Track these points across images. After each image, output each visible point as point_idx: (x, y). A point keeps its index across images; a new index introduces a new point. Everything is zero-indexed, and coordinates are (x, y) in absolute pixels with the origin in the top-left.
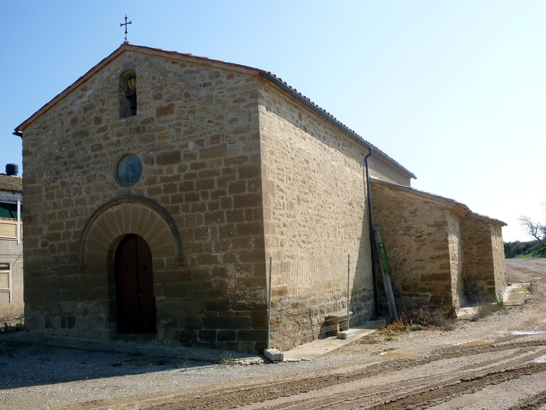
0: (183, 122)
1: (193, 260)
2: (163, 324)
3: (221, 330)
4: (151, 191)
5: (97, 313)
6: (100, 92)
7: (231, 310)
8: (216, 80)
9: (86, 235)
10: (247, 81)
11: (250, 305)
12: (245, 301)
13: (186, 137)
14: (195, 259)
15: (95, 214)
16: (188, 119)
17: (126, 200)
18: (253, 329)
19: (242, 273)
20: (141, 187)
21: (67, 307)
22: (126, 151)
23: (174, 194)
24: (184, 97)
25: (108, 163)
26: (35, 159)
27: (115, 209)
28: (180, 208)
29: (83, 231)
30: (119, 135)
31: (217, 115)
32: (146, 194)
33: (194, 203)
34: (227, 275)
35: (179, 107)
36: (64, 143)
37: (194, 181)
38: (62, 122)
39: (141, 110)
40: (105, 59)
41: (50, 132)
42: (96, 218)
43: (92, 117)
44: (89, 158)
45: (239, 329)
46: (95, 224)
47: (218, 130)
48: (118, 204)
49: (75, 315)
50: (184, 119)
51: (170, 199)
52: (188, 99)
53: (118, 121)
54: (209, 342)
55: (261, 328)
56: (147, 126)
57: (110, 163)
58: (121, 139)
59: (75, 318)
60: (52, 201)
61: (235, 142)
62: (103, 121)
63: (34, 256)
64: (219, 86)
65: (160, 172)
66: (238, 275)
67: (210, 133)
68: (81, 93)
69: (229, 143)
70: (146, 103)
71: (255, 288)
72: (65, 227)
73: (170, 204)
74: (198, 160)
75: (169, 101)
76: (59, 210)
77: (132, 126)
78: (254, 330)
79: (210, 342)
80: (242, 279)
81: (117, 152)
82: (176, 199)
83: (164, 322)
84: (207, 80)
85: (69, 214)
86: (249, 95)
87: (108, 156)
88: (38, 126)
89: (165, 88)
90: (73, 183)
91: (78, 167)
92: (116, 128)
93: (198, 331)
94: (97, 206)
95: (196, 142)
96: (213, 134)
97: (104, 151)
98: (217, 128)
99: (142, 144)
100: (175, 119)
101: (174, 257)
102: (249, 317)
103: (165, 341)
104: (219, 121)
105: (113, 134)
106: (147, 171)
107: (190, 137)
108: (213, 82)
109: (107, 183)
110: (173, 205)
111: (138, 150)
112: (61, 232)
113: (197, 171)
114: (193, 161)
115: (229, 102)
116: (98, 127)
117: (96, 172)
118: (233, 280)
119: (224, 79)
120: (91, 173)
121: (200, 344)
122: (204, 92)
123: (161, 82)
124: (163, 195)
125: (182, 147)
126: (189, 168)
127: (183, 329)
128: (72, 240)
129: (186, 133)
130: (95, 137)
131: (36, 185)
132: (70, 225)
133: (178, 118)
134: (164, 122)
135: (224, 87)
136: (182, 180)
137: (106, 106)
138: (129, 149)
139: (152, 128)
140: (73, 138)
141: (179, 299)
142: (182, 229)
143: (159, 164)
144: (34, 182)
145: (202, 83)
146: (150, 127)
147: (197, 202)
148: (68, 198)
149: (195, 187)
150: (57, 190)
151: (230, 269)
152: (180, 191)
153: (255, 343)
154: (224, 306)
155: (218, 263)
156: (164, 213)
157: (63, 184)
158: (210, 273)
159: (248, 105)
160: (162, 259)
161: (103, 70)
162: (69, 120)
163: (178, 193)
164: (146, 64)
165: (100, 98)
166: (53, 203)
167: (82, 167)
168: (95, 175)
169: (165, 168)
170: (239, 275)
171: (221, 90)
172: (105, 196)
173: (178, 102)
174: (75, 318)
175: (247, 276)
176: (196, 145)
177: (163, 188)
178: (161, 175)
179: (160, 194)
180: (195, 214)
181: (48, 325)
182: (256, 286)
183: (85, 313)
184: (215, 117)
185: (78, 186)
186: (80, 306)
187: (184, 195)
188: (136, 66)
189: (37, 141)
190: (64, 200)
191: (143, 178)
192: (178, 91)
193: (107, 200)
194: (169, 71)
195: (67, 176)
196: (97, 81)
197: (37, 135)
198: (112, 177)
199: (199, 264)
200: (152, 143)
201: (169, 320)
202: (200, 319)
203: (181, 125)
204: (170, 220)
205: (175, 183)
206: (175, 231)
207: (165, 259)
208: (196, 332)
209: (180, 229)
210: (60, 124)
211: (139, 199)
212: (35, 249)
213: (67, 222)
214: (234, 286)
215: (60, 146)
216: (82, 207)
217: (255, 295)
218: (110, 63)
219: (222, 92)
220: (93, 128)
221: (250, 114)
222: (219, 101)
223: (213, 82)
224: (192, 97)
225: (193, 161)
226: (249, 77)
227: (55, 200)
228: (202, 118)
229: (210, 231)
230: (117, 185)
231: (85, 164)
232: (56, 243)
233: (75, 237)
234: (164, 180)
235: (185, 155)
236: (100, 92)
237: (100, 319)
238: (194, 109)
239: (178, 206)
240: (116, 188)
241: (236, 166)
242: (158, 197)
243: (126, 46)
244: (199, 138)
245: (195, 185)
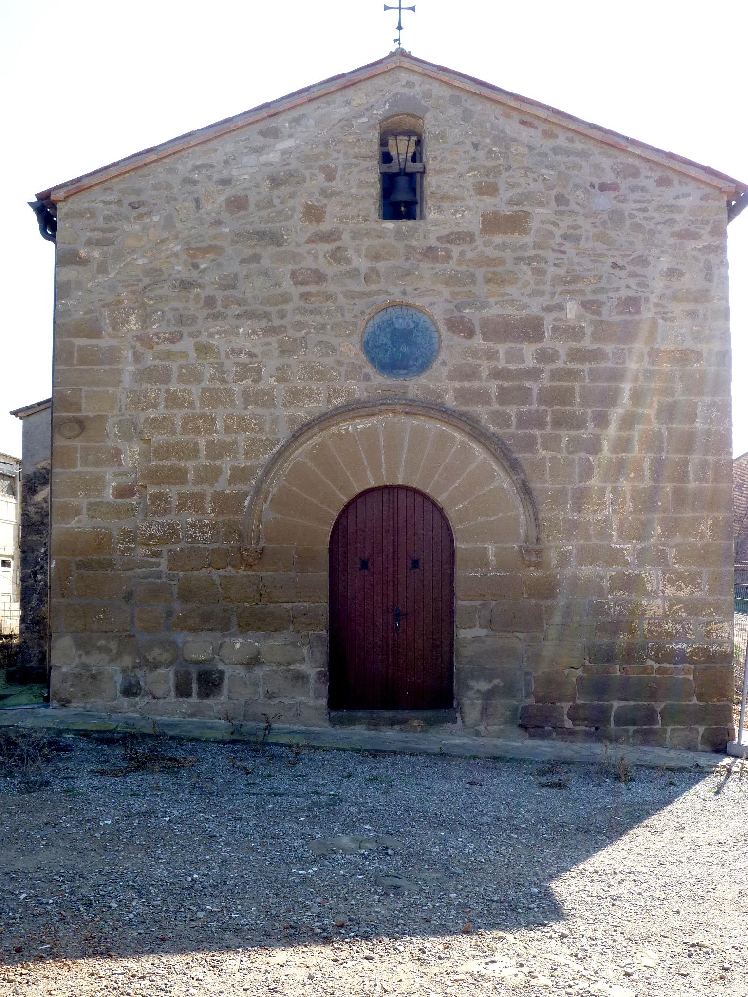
0: (550, 255)
2: (478, 691)
3: (623, 703)
4: (463, 396)
5: (289, 664)
6: (321, 149)
7: (650, 662)
8: (631, 181)
10: (705, 198)
11: (696, 654)
12: (685, 646)
13: (559, 289)
14: (570, 552)
16: (564, 252)
17: (398, 408)
18: (697, 702)
19: (680, 589)
20: (438, 381)
21: (199, 648)
22: (398, 297)
24: (553, 203)
25: (343, 315)
26: (100, 279)
27: (361, 425)
28: (539, 441)
30: (376, 257)
31: (635, 255)
32: (450, 401)
33: (573, 433)
34: (646, 589)
35: (543, 222)
36: (206, 250)
37: (577, 385)
38: (197, 200)
39: (440, 210)
40: (343, 76)
41: (156, 218)
43: (299, 203)
44: (286, 298)
45: (667, 702)
46: (300, 454)
47: (635, 288)
48: (373, 415)
49: (221, 667)
50: (554, 250)
51: (514, 420)
52: (563, 208)
53: (374, 225)
54: (593, 729)
55: (718, 701)
56: (455, 250)
57: (348, 317)
58: (381, 265)
59: (222, 673)
60: (163, 387)
61: (675, 318)
62: (327, 217)
63: (92, 518)
64: (637, 195)
65: (491, 355)
66: (671, 591)
67: (618, 289)
68: (259, 141)
69: (663, 318)
70: (456, 198)
71: (707, 619)
72: (202, 453)
73: (513, 429)
74: (587, 343)
75: (517, 204)
76: (188, 412)
77: (415, 243)
78: (702, 704)
79: (597, 729)
80: (679, 601)
81: (368, 295)
83: (483, 686)
84: (609, 177)
85: (219, 425)
86: (708, 228)
87: (341, 300)
88: (113, 197)
89: (505, 174)
90: (236, 352)
91: (252, 315)
92: (365, 240)
93: (566, 706)
94: (309, 413)
95: (585, 305)
96: (624, 293)
97: (330, 287)
98: (632, 282)
99: (440, 287)
100: (531, 245)
102: (691, 677)
103: (481, 728)
104: (639, 269)
105: (357, 251)
106: (451, 352)
107: (569, 292)
108: (625, 184)
109: (340, 363)
110: (522, 432)
111: (432, 299)
112: (190, 464)
113: (585, 367)
115: (660, 232)
116: (313, 229)
117: (308, 333)
118: (659, 601)
119: (650, 184)
120: (292, 333)
121: (572, 733)
122: (603, 202)
123: (497, 158)
124: (495, 406)
125: (548, 309)
126: (563, 357)
128: (222, 485)
129: (557, 280)
130: (302, 250)
131: (104, 342)
132: (217, 450)
133: (536, 246)
134: (503, 246)
135: (650, 201)
136: (546, 379)
137: (337, 185)
138: (404, 293)
139: (469, 255)
140: (234, 243)
141: (521, 636)
142: (540, 485)
143: (486, 337)
144: (95, 332)
145: (597, 181)
146: (462, 253)
148: (217, 384)
149: (577, 400)
150: (182, 362)
151: (653, 576)
153: (701, 729)
154: (632, 655)
155: (626, 563)
156: (501, 450)
157: (204, 350)
158: (606, 584)
159: (705, 247)
160: (483, 546)
161: (329, 98)
162: (221, 199)
163: (534, 407)
164: (452, 111)
165: (321, 163)
166: (167, 391)
167: (267, 315)
168: (304, 340)
169: (502, 348)
170: (674, 591)
171: (643, 206)
173: (541, 210)
174: (222, 673)
175: (691, 593)
176: (583, 310)
177: (494, 392)
179: (488, 403)
180: (576, 456)
181: (130, 690)
182: (711, 615)
183: (254, 661)
184: (627, 259)
186: (238, 646)
188: (427, 110)
189: (107, 235)
190: (204, 390)
191: (444, 363)
192: (540, 186)
193: (339, 401)
194: (515, 140)
195: (219, 333)
196: (311, 122)
197: (108, 218)
199: (580, 564)
200: (466, 289)
201: (496, 682)
202: (574, 679)
203: (546, 262)
204: (513, 466)
205: (528, 384)
206: (525, 490)
207: (491, 548)
208: (563, 708)
209: (536, 485)
210: (191, 205)
212: (92, 500)
213: (210, 444)
214: (660, 612)
215: (193, 257)
216: (260, 411)
217: (709, 634)
218: (352, 89)
219: (645, 210)
220: (297, 230)
221: (709, 267)
222: (637, 227)
223: (625, 184)
224: (573, 206)
226: (708, 190)
227: (174, 386)
228: (600, 255)
229: (608, 495)
230: (369, 369)
231: (273, 309)
232: (173, 493)
233: (232, 480)
234: (497, 374)
235: (555, 329)
236: (321, 149)
237: (300, 678)
238: (578, 232)
239: (534, 437)
240: (367, 377)
241: (675, 368)
242: (481, 412)
243: (403, 59)
244: (590, 297)
245: (577, 396)
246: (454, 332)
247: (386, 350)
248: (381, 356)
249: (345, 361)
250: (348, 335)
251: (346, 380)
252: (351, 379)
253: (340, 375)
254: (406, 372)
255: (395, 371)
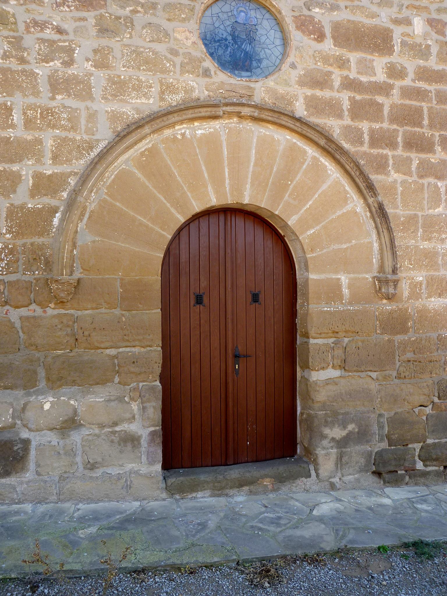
1: (415, 286)
2: (333, 439)
5: (115, 424)
14: (421, 283)
23: (376, 126)
27: (202, 129)
28: (391, 162)
32: (300, 109)
33: (423, 156)
46: (125, 161)
48: (215, 117)
49: (25, 434)
51: (366, 137)
59: (26, 443)
65: (343, 63)
73: (365, 148)
82: (376, 140)
93: (417, 446)
94: (138, 110)
95: (431, 22)
109: (174, 52)
110: (375, 151)
113: (432, 88)
114: (421, 62)
121: (424, 474)
124: (347, 121)
125: (397, 22)
126: (411, 75)
127: (384, 445)
141: (374, 375)
142: (396, 211)
147: (429, 155)
149: (426, 122)
163: (385, 125)
169: (353, 57)
172: (167, 88)
174: (26, 443)
176: (429, 28)
177: (346, 105)
178: (345, 73)
179: (340, 116)
185: (57, 37)
186: (47, 406)
191: (293, 66)
193: (174, 99)
198: (195, 38)
201: (351, 427)
204: (366, 187)
205: (380, 99)
207: (344, 279)
211: (277, 115)
225: (421, 62)
230: (209, 63)
234: (350, 84)
240: (206, 73)
242: (335, 126)
245: (426, 117)
246: (303, 32)
247: (227, 47)
248: (220, 52)
249: (181, 51)
250: (184, 20)
251: (182, 73)
252: (188, 72)
253: (174, 66)
254: (249, 74)
255: (236, 72)
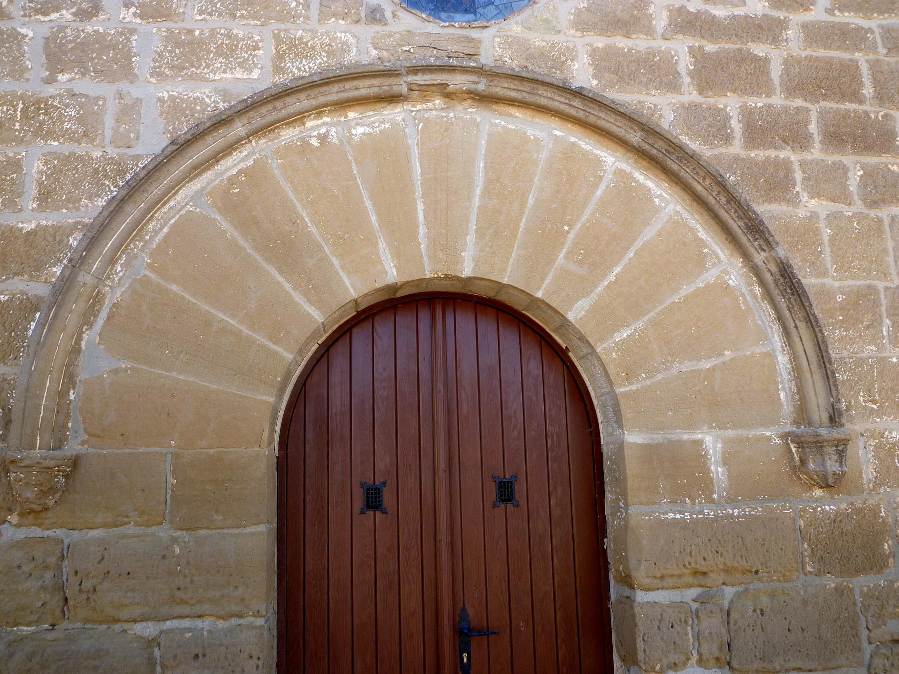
9: (112, 261)
15: (198, 139)
23: (759, 102)
27: (362, 125)
28: (798, 176)
29: (95, 235)
33: (872, 160)
42: (216, 157)
46: (190, 197)
48: (393, 99)
73: (737, 148)
82: (759, 130)
94: (225, 94)
101: (772, 433)
124: (690, 95)
142: (823, 280)
149: (868, 90)
152: (794, 87)
177: (685, 64)
187: (814, 114)
193: (302, 68)
204: (745, 229)
205: (759, 49)
207: (712, 442)
211: (533, 90)
216: (89, 86)
240: (375, 16)
